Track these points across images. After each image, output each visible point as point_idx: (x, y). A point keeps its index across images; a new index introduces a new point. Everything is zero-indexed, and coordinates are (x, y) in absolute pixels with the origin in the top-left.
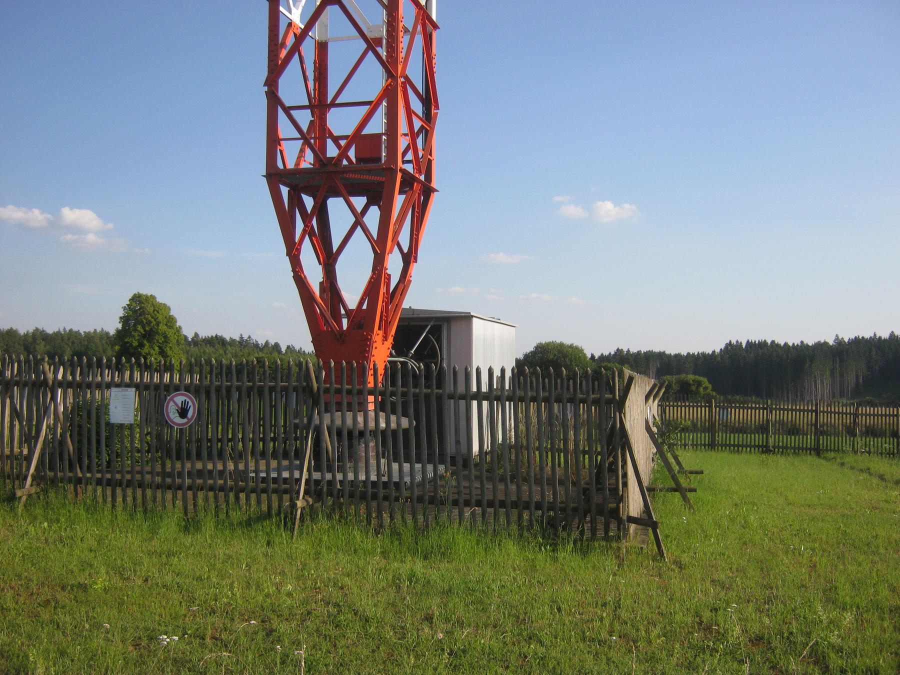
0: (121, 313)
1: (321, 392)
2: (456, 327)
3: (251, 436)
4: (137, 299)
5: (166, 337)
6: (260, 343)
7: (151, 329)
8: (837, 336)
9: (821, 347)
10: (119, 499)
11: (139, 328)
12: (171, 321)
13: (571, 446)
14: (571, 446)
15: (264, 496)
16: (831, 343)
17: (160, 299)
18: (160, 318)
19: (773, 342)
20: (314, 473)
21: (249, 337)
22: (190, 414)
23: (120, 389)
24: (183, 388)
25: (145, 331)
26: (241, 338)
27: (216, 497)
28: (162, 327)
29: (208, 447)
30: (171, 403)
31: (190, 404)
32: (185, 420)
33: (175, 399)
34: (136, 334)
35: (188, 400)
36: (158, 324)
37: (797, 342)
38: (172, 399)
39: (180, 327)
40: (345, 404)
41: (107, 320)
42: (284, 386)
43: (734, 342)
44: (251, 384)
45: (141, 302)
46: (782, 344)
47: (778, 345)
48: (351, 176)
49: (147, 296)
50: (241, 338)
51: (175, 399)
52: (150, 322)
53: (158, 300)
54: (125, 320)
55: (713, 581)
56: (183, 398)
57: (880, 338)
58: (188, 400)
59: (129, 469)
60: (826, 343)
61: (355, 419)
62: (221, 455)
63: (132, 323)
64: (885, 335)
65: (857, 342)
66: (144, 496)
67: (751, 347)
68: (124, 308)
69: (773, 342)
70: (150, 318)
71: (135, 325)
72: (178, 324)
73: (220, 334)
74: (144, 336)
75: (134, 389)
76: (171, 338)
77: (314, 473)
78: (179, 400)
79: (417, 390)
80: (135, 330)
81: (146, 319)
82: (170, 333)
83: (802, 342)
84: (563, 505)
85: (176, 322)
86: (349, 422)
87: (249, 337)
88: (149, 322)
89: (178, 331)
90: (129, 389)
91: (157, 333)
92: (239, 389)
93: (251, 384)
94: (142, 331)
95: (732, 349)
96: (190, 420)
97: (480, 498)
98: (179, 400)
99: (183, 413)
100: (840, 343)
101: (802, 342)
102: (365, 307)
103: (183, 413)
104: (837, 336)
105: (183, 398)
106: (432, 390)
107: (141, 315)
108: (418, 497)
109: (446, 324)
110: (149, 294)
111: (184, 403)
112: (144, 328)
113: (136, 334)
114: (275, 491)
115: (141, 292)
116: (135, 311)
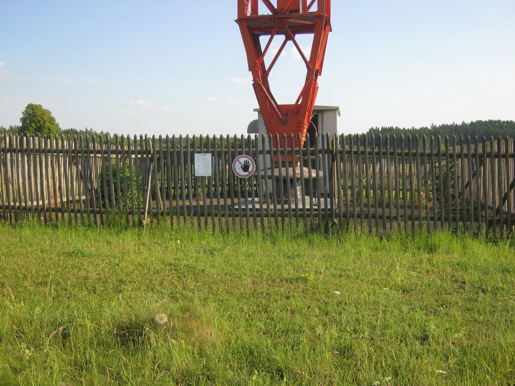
0: (21, 116)
1: (338, 153)
2: (326, 116)
3: (214, 183)
4: (30, 107)
5: (49, 129)
6: (97, 132)
7: (40, 125)
9: (424, 130)
10: (203, 225)
11: (33, 125)
12: (52, 120)
13: (378, 182)
14: (378, 182)
15: (258, 219)
16: (429, 128)
17: (45, 107)
18: (46, 118)
19: (397, 127)
21: (91, 129)
22: (250, 169)
23: (201, 154)
24: (244, 153)
25: (36, 126)
26: (87, 130)
27: (82, 217)
28: (47, 124)
29: (166, 192)
30: (237, 163)
31: (250, 162)
32: (247, 173)
34: (31, 128)
35: (248, 160)
36: (44, 123)
37: (410, 127)
38: (238, 160)
39: (58, 124)
40: (281, 163)
41: (13, 119)
42: (312, 150)
43: (374, 128)
45: (33, 109)
46: (402, 129)
47: (399, 129)
48: (292, 20)
49: (36, 105)
50: (87, 130)
52: (39, 121)
53: (43, 107)
54: (23, 120)
56: (245, 159)
57: (457, 125)
58: (248, 160)
59: (137, 207)
60: (426, 128)
61: (287, 171)
62: (188, 197)
63: (28, 122)
64: (459, 123)
65: (444, 127)
67: (384, 131)
68: (23, 113)
69: (397, 127)
70: (39, 119)
71: (30, 123)
72: (56, 122)
73: (73, 128)
74: (36, 130)
75: (211, 154)
76: (53, 130)
78: (242, 160)
80: (31, 126)
81: (37, 119)
82: (52, 127)
83: (413, 128)
84: (131, 210)
85: (55, 121)
86: (284, 173)
87: (91, 129)
88: (39, 121)
89: (57, 126)
90: (207, 154)
91: (45, 128)
92: (282, 153)
93: (290, 149)
94: (35, 126)
95: (373, 132)
96: (250, 173)
97: (374, 213)
98: (242, 160)
99: (245, 168)
100: (434, 128)
101: (413, 128)
102: (299, 103)
104: (432, 124)
105: (245, 159)
107: (33, 117)
108: (372, 214)
109: (320, 115)
110: (38, 104)
112: (36, 125)
113: (31, 128)
114: (252, 216)
115: (33, 103)
116: (30, 115)
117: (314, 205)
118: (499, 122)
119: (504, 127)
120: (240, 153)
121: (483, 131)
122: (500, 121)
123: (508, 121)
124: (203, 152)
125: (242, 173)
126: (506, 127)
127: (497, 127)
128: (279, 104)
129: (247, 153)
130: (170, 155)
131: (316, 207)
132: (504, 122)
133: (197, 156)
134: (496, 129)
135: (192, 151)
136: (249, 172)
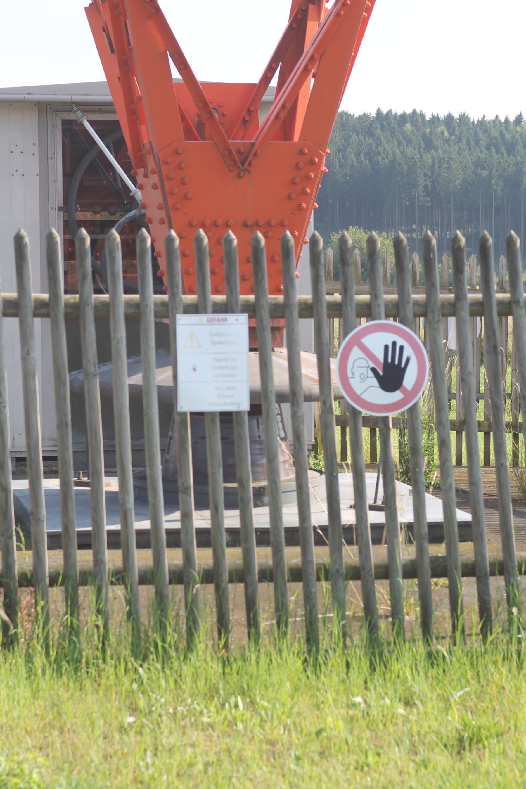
8: (497, 117)
10: (237, 616)
20: (47, 553)
22: (409, 379)
27: (309, 599)
30: (356, 353)
31: (408, 352)
32: (397, 396)
33: (367, 340)
35: (400, 342)
38: (357, 342)
44: (281, 298)
51: (367, 340)
55: (141, 782)
56: (388, 338)
66: (309, 599)
77: (47, 553)
78: (377, 341)
79: (105, 297)
90: (231, 318)
93: (281, 298)
99: (390, 376)
103: (390, 376)
105: (388, 338)
106: (114, 296)
111: (392, 349)
117: (373, 508)
118: (415, 118)
119: (437, 143)
120: (367, 311)
121: (358, 154)
122: (422, 116)
123: (449, 118)
124: (210, 308)
125: (375, 395)
126: (447, 141)
127: (409, 141)
128: (202, 75)
129: (396, 311)
130: (252, 330)
131: (376, 517)
132: (435, 119)
133: (186, 326)
134: (409, 151)
135: (164, 304)
136: (405, 391)
